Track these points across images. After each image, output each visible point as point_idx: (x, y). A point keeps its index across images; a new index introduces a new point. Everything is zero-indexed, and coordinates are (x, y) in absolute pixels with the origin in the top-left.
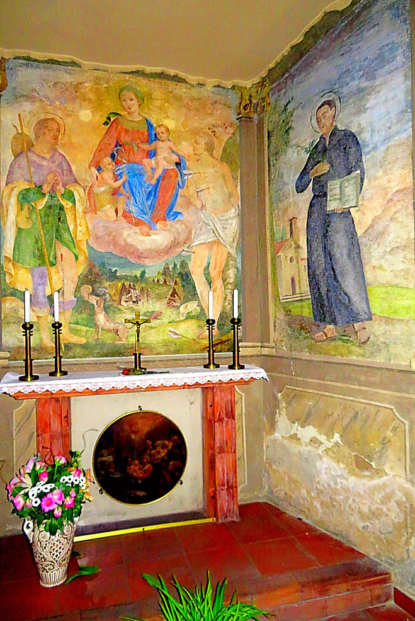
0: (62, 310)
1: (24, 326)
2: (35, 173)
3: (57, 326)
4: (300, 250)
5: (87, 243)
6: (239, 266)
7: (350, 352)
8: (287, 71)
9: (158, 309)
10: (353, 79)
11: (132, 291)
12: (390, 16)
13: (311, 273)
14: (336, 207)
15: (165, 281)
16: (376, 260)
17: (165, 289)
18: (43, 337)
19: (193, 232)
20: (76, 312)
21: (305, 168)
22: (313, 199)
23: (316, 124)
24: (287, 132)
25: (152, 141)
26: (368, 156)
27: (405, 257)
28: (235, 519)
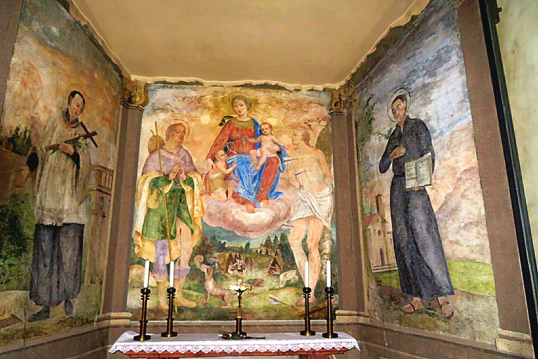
1: (142, 291)
2: (164, 165)
4: (386, 224)
5: (202, 220)
6: (334, 238)
7: (437, 327)
8: (367, 74)
9: (260, 278)
10: (418, 77)
11: (238, 260)
12: (443, 26)
13: (396, 246)
14: (413, 185)
15: (267, 252)
16: (452, 235)
17: (267, 259)
19: (292, 209)
20: (190, 278)
22: (393, 179)
23: (391, 115)
24: (370, 122)
25: (258, 136)
26: (437, 140)
27: (478, 233)
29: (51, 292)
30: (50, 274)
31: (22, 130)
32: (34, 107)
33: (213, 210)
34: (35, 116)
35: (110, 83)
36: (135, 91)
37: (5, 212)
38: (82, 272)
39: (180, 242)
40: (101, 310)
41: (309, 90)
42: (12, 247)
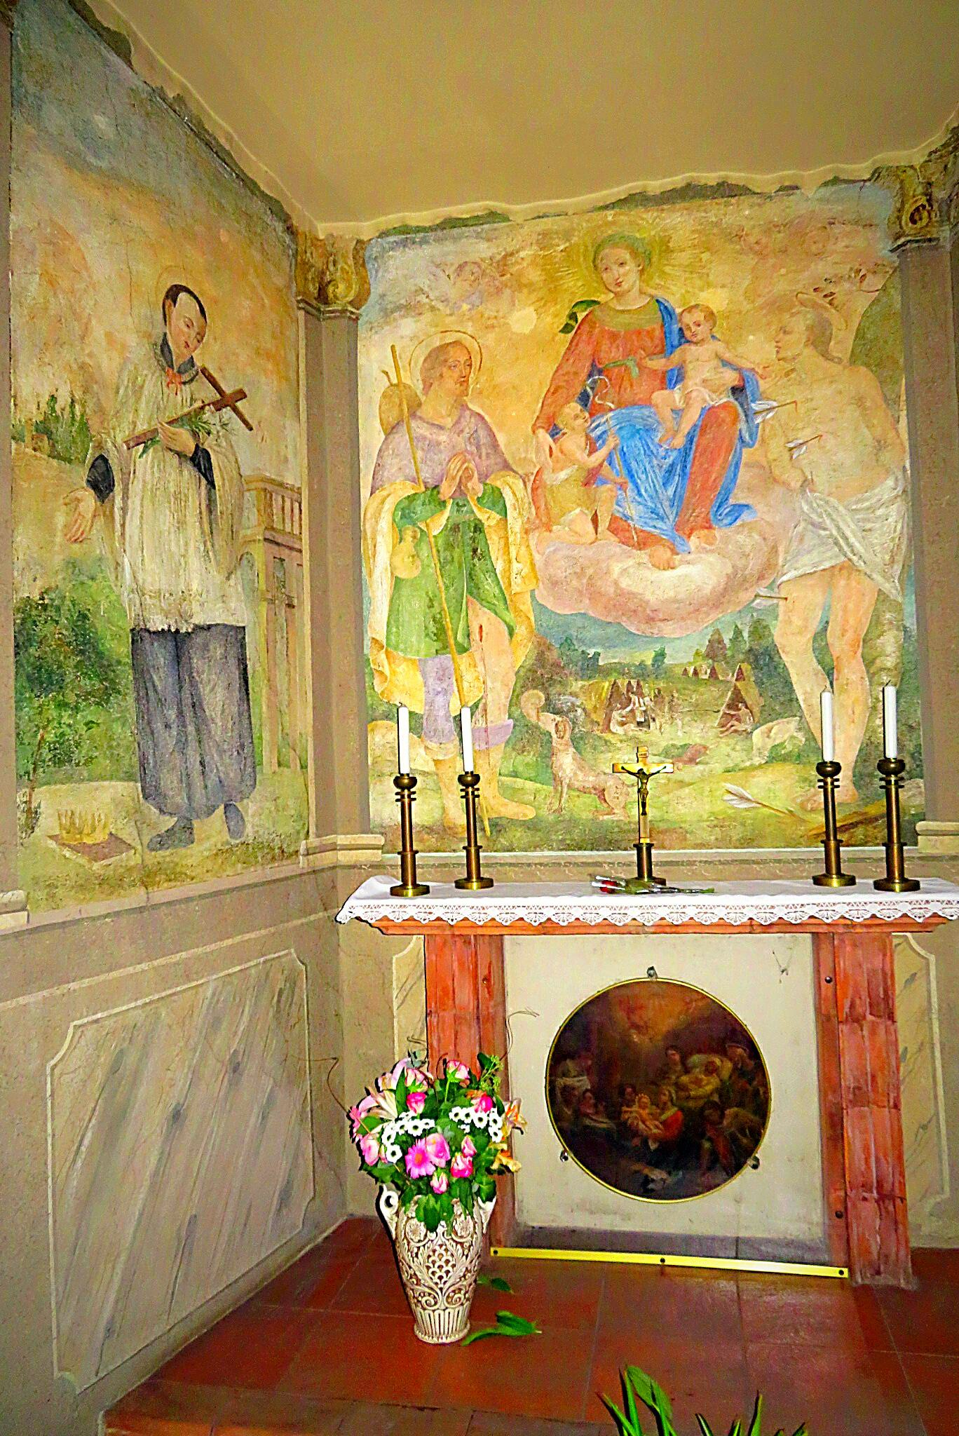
1: (397, 782)
2: (424, 461)
5: (533, 597)
6: (911, 623)
9: (698, 741)
11: (634, 698)
15: (713, 673)
17: (715, 691)
18: (437, 805)
19: (781, 549)
28: (903, 1284)
29: (189, 785)
30: (182, 745)
31: (63, 400)
32: (83, 338)
33: (561, 569)
34: (87, 360)
35: (263, 251)
36: (332, 268)
37: (56, 602)
38: (256, 741)
39: (483, 660)
40: (312, 830)
41: (826, 184)
42: (86, 683)
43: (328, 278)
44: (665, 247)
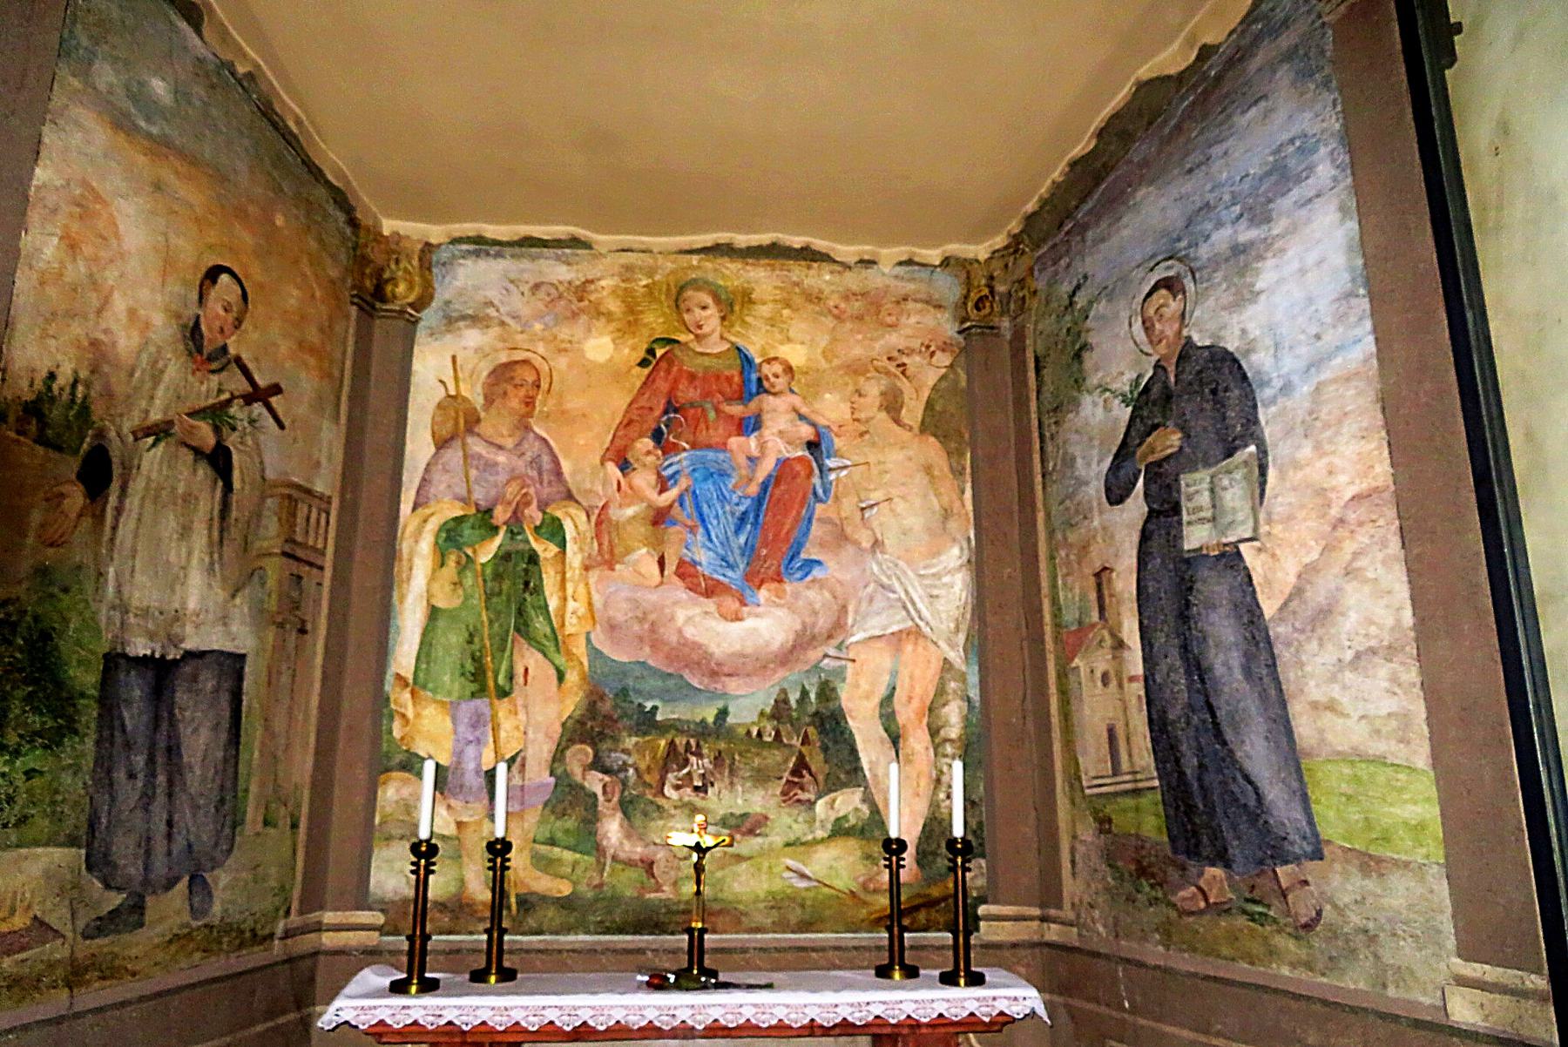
0: (516, 807)
1: (415, 848)
2: (477, 481)
3: (499, 849)
4: (1126, 654)
5: (588, 641)
6: (974, 693)
7: (1272, 953)
9: (758, 810)
10: (1219, 225)
11: (693, 759)
12: (1292, 75)
13: (1155, 717)
16: (1317, 685)
19: (851, 608)
21: (1124, 444)
22: (1146, 522)
23: (1141, 336)
24: (1078, 356)
25: (751, 396)
26: (1273, 409)
27: (1394, 679)
29: (148, 853)
30: (147, 799)
31: (63, 379)
32: (99, 312)
33: (620, 612)
34: (102, 337)
35: (321, 241)
36: (393, 266)
37: (14, 618)
38: (240, 794)
39: (526, 707)
40: (295, 906)
41: (900, 264)
42: (35, 721)
43: (386, 275)
44: (746, 298)
